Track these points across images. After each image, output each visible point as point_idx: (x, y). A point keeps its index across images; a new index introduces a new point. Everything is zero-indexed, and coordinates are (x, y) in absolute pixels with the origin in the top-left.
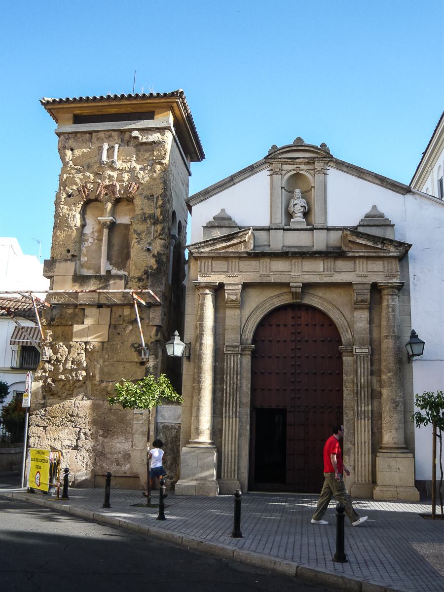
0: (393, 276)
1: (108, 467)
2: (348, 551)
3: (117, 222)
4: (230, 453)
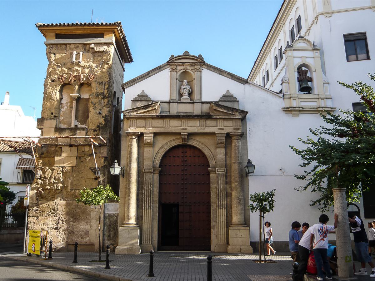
0: (238, 129)
1: (75, 240)
3: (81, 97)
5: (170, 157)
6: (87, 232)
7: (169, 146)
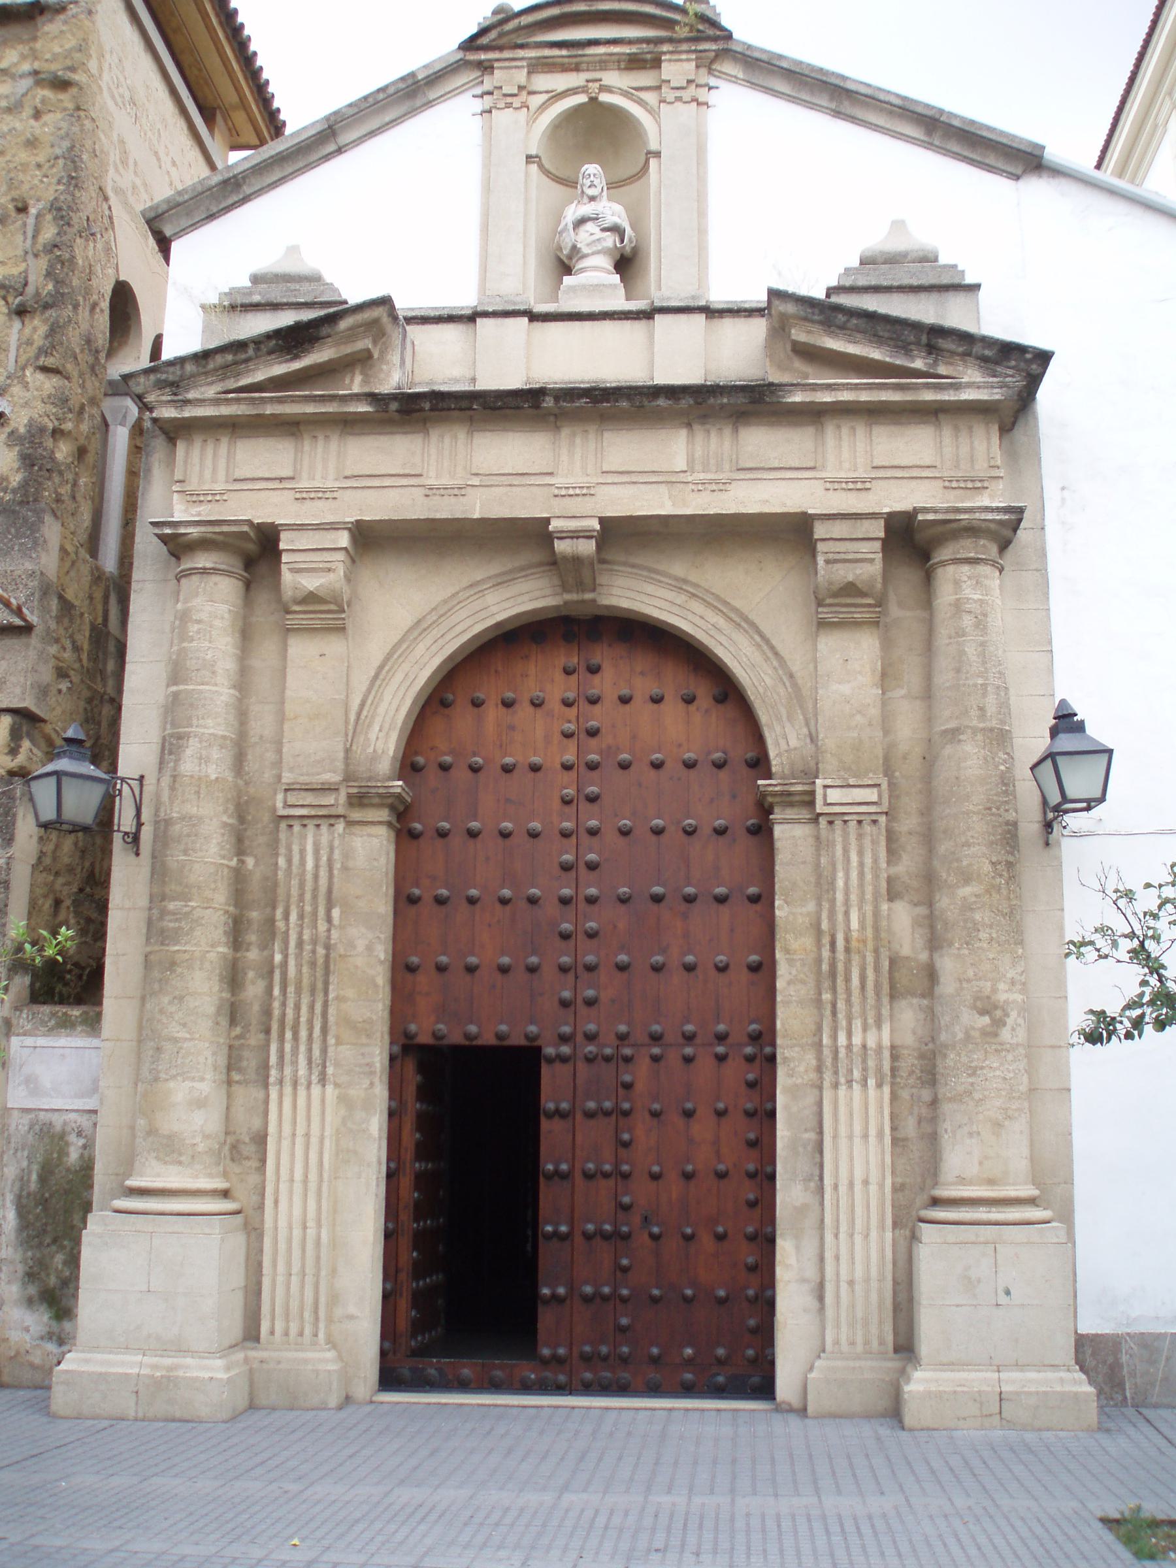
0: (977, 485)
4: (297, 1233)
5: (477, 704)
7: (469, 622)
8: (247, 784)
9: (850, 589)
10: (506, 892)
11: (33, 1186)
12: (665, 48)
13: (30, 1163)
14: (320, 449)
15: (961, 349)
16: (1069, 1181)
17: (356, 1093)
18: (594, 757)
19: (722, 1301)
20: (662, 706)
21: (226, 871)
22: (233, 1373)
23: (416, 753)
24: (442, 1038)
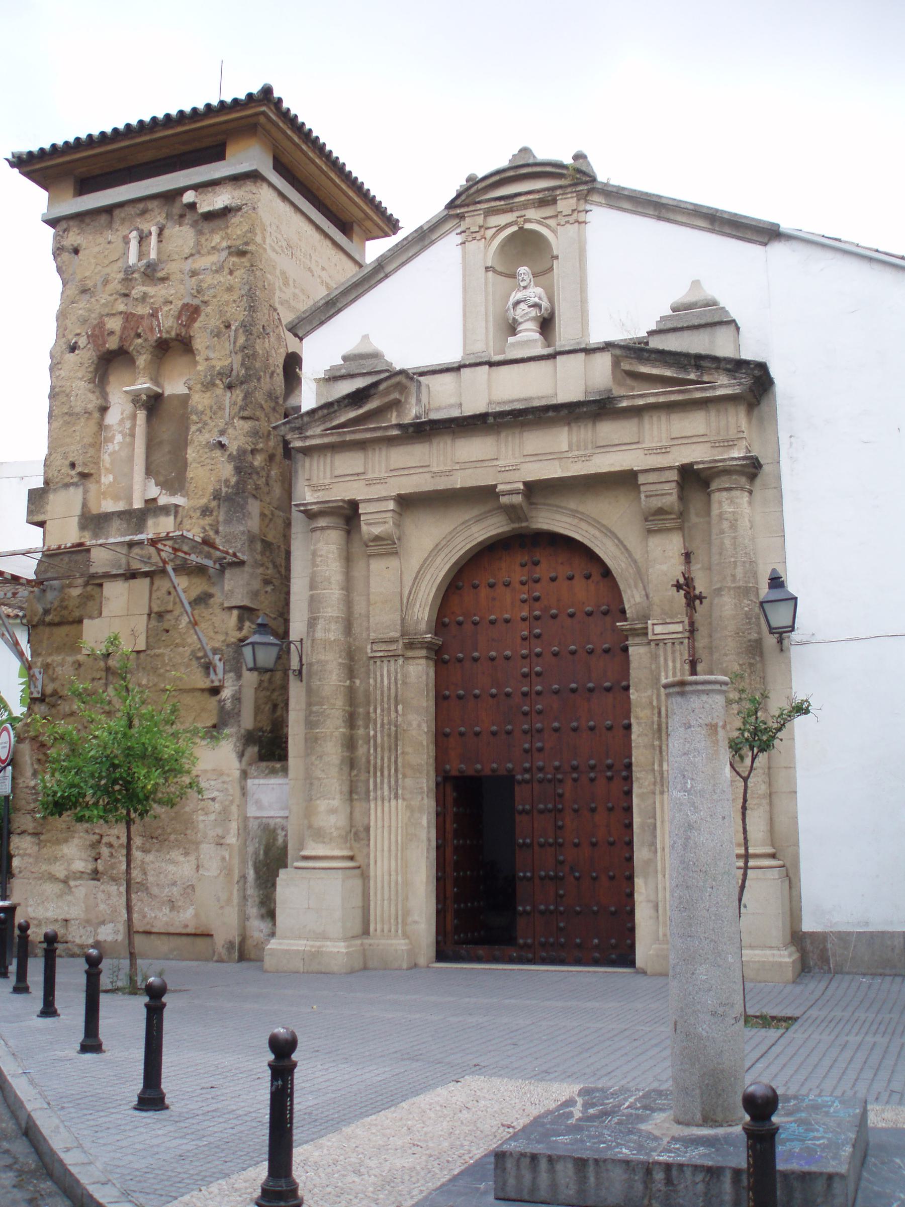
0: (730, 444)
1: (153, 915)
2: (167, 1085)
3: (167, 393)
4: (386, 877)
6: (188, 887)
7: (463, 543)
8: (354, 640)
9: (660, 511)
10: (494, 691)
11: (261, 857)
12: (558, 192)
13: (260, 844)
14: (377, 455)
15: (714, 366)
16: (796, 844)
17: (415, 803)
18: (537, 613)
19: (613, 914)
20: (574, 581)
21: (342, 688)
22: (351, 949)
23: (445, 617)
24: (464, 772)
